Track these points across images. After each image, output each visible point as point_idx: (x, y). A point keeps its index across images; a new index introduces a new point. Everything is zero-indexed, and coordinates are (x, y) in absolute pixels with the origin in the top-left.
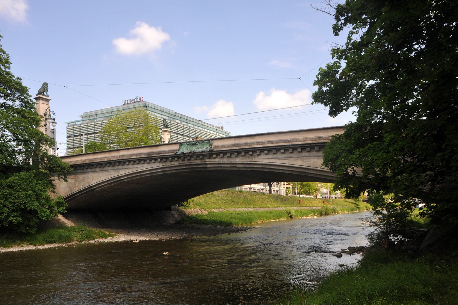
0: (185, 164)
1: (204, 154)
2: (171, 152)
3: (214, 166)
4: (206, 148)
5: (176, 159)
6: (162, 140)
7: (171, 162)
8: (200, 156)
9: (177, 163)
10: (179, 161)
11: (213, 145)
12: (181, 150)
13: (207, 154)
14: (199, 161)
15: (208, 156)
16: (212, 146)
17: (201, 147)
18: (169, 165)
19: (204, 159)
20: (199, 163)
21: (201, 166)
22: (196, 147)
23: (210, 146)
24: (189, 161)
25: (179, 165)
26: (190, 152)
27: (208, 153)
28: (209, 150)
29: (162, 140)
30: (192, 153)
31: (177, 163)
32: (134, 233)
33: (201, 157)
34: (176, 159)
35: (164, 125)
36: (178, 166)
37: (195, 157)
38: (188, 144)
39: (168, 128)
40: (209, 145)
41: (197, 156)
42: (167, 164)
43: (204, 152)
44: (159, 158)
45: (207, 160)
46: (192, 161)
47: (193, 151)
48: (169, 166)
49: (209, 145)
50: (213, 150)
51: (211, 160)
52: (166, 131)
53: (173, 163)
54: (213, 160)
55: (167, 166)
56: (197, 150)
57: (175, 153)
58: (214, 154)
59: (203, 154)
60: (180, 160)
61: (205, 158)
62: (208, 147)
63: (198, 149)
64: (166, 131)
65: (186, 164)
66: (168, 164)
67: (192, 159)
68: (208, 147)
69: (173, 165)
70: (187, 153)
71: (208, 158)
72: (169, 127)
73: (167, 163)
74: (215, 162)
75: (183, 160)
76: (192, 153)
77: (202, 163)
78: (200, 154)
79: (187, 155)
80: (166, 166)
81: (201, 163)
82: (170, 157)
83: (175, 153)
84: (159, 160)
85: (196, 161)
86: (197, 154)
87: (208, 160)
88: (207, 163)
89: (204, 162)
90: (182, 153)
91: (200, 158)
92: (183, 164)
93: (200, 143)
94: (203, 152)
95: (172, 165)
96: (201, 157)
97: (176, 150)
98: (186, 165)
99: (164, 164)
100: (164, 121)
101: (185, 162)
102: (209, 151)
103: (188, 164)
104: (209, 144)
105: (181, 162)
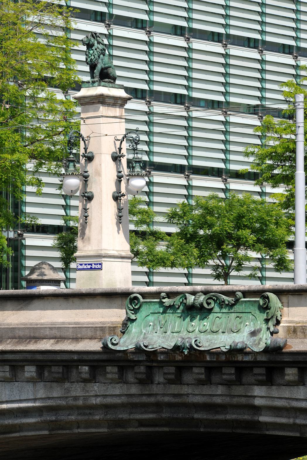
0: (152, 400)
1: (243, 362)
2: (90, 334)
3: (291, 421)
4: (253, 334)
5: (112, 370)
6: (82, 151)
7: (89, 385)
8: (225, 370)
9: (118, 392)
10: (126, 382)
11: (284, 319)
12: (134, 328)
13: (256, 364)
14: (220, 390)
15: (262, 371)
16: (278, 322)
17: (230, 325)
18: (76, 398)
19: (241, 384)
20: (218, 400)
21: (230, 416)
22: (206, 324)
23: (271, 324)
24: (174, 389)
25: (124, 399)
26: (177, 348)
27: (259, 358)
28: (261, 347)
29: (82, 151)
30: (186, 352)
31: (117, 390)
32: (69, 359)
33: (229, 373)
34: (112, 370)
35: (93, 67)
36: (123, 406)
37: (198, 372)
38: (170, 307)
39: (114, 79)
40: (267, 321)
41: (210, 365)
42: (68, 390)
43: (241, 351)
44: (31, 362)
45: (258, 391)
46: (185, 390)
47: (191, 346)
48: (80, 402)
49: (267, 321)
50: (285, 345)
51: (275, 392)
52: (102, 100)
53: (96, 388)
54: (287, 392)
55: (71, 402)
56: (209, 337)
57: (105, 347)
58: (291, 364)
59: (238, 362)
60: (130, 377)
61: (247, 378)
62: (259, 331)
63: (215, 336)
64: (102, 100)
65: (160, 399)
66: (74, 394)
67: (187, 377)
68: (259, 331)
69: (98, 401)
70: (166, 352)
71: (260, 383)
72: (118, 73)
73: (67, 385)
74: (295, 404)
75: (141, 382)
76: (186, 352)
77: (235, 400)
78: (223, 358)
79: (161, 357)
80: (63, 403)
81: (227, 400)
82: (83, 362)
83: (105, 347)
84: (30, 371)
85: (207, 390)
86: (208, 358)
87: (264, 388)
88: (258, 402)
89: (243, 400)
90: (138, 350)
91: (224, 377)
92: (145, 399)
93: (221, 307)
94: (234, 351)
95: (94, 401)
96: (229, 373)
97: (112, 329)
98: (159, 406)
99: (57, 391)
100: (90, 46)
101: (155, 389)
102: (267, 350)
103: (166, 399)
104: (265, 316)
105: (134, 390)
